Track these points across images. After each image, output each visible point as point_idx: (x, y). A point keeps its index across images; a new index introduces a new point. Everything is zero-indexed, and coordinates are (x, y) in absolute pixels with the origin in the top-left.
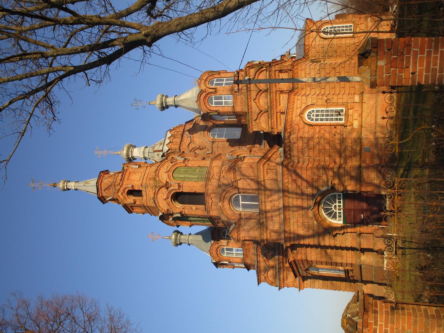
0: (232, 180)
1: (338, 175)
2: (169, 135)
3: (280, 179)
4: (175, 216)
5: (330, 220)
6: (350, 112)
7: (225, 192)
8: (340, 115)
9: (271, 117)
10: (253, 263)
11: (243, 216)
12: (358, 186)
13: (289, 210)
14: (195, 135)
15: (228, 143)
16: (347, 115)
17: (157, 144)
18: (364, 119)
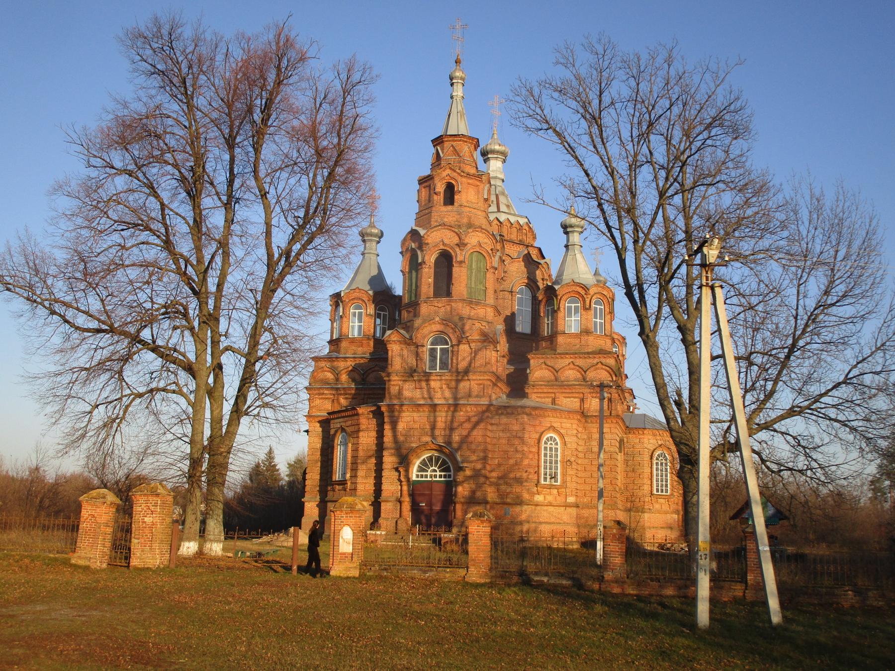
0: (470, 338)
1: (477, 474)
2: (522, 221)
3: (472, 401)
4: (419, 252)
5: (417, 463)
6: (555, 491)
7: (453, 326)
8: (551, 478)
9: (549, 386)
10: (342, 350)
11: (420, 349)
12: (462, 500)
13: (429, 411)
14: (523, 263)
15: (509, 314)
16: (551, 487)
17: (507, 200)
18: (545, 508)
